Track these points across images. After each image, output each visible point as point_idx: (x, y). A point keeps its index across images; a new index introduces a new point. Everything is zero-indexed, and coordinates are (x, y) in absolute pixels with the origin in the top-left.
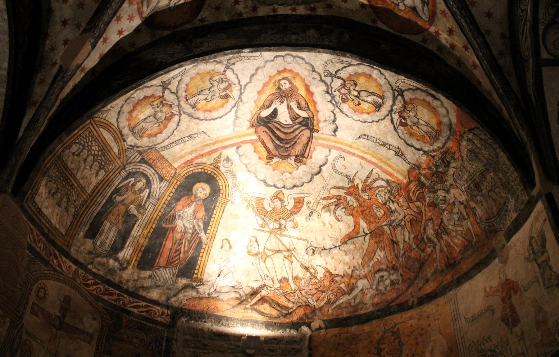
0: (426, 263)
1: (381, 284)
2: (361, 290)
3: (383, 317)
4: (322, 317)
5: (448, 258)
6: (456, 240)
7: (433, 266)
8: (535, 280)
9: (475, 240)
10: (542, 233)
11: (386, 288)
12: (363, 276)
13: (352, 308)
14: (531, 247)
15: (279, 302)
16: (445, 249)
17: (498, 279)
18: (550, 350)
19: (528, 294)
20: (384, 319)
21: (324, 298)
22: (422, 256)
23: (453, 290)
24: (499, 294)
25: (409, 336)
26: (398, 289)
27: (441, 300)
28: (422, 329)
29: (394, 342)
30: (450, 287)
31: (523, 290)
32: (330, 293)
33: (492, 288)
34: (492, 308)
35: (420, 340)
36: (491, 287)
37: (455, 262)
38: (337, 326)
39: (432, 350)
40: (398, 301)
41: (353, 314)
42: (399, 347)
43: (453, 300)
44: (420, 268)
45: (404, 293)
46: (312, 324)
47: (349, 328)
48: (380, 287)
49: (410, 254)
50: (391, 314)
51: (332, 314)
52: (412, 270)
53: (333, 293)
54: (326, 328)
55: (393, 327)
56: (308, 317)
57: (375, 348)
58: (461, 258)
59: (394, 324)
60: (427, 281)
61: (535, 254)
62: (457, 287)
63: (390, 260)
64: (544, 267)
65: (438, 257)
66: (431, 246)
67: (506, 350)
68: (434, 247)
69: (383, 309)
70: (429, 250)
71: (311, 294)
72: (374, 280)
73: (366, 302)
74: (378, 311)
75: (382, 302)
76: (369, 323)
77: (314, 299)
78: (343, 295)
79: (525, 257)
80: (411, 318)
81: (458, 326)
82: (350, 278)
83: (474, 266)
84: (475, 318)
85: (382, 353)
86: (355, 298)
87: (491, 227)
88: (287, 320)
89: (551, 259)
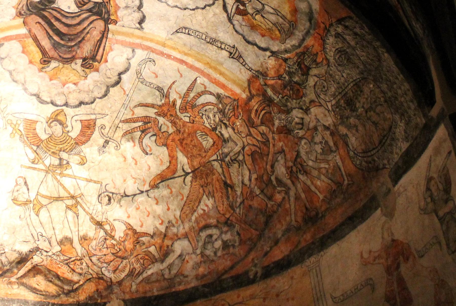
0: (275, 216)
1: (209, 246)
3: (212, 295)
5: (307, 209)
6: (319, 183)
7: (285, 220)
9: (346, 182)
11: (215, 253)
12: (182, 235)
13: (165, 281)
14: (429, 193)
16: (303, 196)
19: (424, 262)
20: (213, 298)
21: (125, 267)
22: (269, 206)
23: (315, 256)
26: (234, 254)
31: (416, 256)
32: (133, 260)
33: (372, 253)
34: (371, 282)
36: (370, 252)
37: (317, 214)
40: (233, 273)
41: (168, 291)
43: (314, 271)
44: (266, 223)
45: (243, 259)
49: (251, 203)
50: (223, 290)
51: (137, 291)
53: (138, 261)
56: (101, 296)
58: (327, 209)
60: (276, 242)
63: (222, 212)
64: (447, 222)
65: (293, 207)
68: (287, 193)
69: (212, 283)
70: (279, 197)
71: (106, 261)
73: (186, 273)
74: (204, 286)
75: (210, 273)
77: (111, 268)
78: (153, 263)
79: (419, 208)
82: (164, 238)
86: (170, 267)
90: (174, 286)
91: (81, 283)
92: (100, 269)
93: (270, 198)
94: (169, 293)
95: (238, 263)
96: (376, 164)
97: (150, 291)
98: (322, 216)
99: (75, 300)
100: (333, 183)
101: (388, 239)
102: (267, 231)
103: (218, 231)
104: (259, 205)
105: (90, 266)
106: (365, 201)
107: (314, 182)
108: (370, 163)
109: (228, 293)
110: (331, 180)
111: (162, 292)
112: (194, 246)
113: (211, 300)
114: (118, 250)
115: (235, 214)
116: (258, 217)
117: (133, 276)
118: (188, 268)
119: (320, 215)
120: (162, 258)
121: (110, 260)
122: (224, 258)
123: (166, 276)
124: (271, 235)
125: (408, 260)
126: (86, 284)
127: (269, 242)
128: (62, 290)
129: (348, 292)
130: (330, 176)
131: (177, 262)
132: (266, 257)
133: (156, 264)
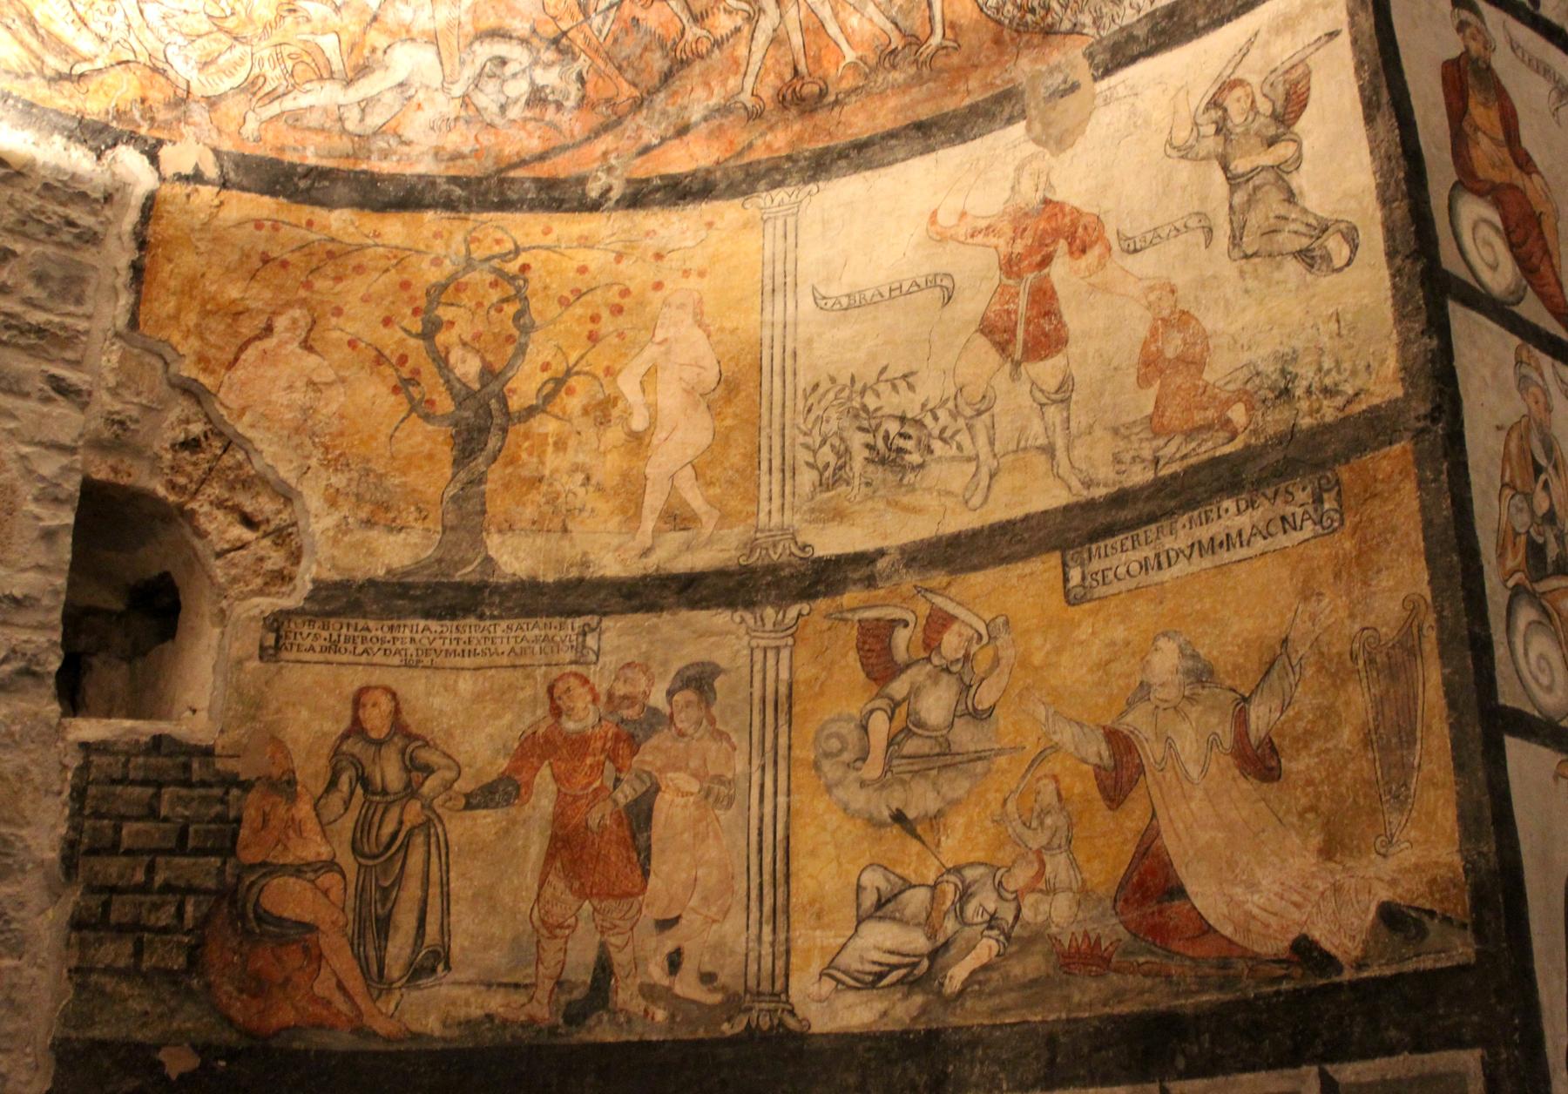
0: (698, 67)
1: (491, 86)
2: (401, 85)
3: (469, 206)
4: (214, 139)
5: (796, 72)
6: (854, 21)
7: (724, 83)
8: (1193, 223)
9: (936, 40)
10: (1295, 75)
11: (503, 108)
12: (423, 33)
13: (345, 139)
14: (1215, 114)
15: (37, 14)
16: (797, 39)
17: (1006, 194)
18: (1184, 451)
19: (1145, 265)
20: (472, 216)
21: (236, 65)
22: (689, 36)
23: (790, 190)
24: (993, 240)
25: (565, 303)
26: (554, 126)
27: (727, 211)
28: (625, 293)
29: (500, 310)
30: (778, 177)
31: (1115, 247)
32: (266, 53)
33: (969, 219)
34: (946, 282)
35: (607, 324)
36: (963, 214)
37: (823, 94)
38: (270, 189)
39: (652, 372)
40: (543, 170)
41: (345, 165)
42: (516, 333)
43: (780, 223)
44: (667, 77)
45: (577, 145)
46: (165, 153)
47: (320, 214)
48: (481, 96)
49: (640, 14)
50: (504, 205)
51: (258, 139)
52: (630, 74)
53: (279, 59)
54: (225, 184)
55: (503, 257)
56: (152, 119)
57: (416, 312)
58: (855, 90)
59: (509, 246)
60: (683, 131)
61: (1227, 140)
62: (806, 183)
63: (552, 11)
64: (1256, 189)
65: (757, 57)
66: (737, 10)
67: (970, 428)
68: (752, 19)
69: (480, 180)
70: (723, 23)
71: (185, 30)
72: (462, 63)
73: (408, 134)
74: (454, 180)
75: (476, 153)
76: (407, 216)
77: (196, 52)
78: (321, 78)
79: (1169, 142)
80: (586, 242)
81: (779, 317)
82: (370, 24)
83: (907, 127)
84: (855, 303)
85: (441, 338)
86: (365, 106)
87: (1032, 11)
88: (60, 102)
89: (1304, 166)
90: (369, 158)
91: (99, 64)
92: (162, 47)
93: (698, 18)
94: (349, 172)
95: (564, 148)
96: (1049, 20)
97: (295, 149)
98: (836, 102)
99: (72, 106)
100: (896, 32)
101: (1030, 195)
102: (662, 95)
103: (526, 52)
104: (661, 24)
105: (134, 25)
106: (978, 97)
107: (842, 15)
108: (1032, 11)
109: (518, 217)
110: (896, 24)
111: (328, 163)
112: (448, 72)
113: (466, 219)
114: (228, 12)
115: (587, 29)
116: (648, 55)
117: (254, 94)
118: (417, 127)
119: (831, 98)
120: (351, 75)
121: (195, 32)
122: (523, 128)
123: (351, 126)
124: (671, 109)
125: (1084, 251)
126: (113, 71)
127: (659, 123)
128: (38, 64)
129: (868, 294)
130: (893, 12)
131: (388, 97)
132: (644, 157)
133: (328, 85)
